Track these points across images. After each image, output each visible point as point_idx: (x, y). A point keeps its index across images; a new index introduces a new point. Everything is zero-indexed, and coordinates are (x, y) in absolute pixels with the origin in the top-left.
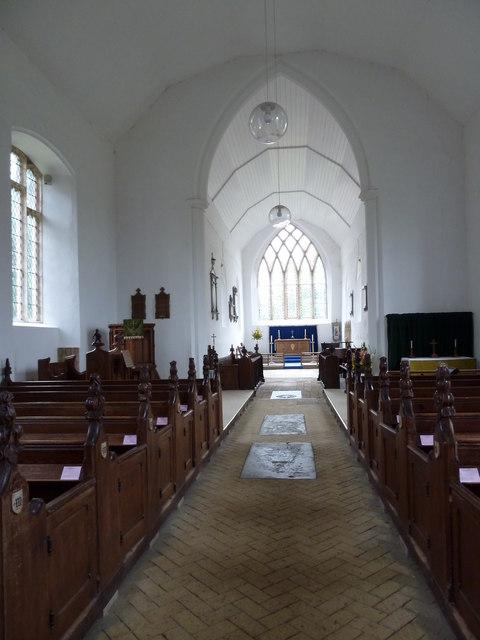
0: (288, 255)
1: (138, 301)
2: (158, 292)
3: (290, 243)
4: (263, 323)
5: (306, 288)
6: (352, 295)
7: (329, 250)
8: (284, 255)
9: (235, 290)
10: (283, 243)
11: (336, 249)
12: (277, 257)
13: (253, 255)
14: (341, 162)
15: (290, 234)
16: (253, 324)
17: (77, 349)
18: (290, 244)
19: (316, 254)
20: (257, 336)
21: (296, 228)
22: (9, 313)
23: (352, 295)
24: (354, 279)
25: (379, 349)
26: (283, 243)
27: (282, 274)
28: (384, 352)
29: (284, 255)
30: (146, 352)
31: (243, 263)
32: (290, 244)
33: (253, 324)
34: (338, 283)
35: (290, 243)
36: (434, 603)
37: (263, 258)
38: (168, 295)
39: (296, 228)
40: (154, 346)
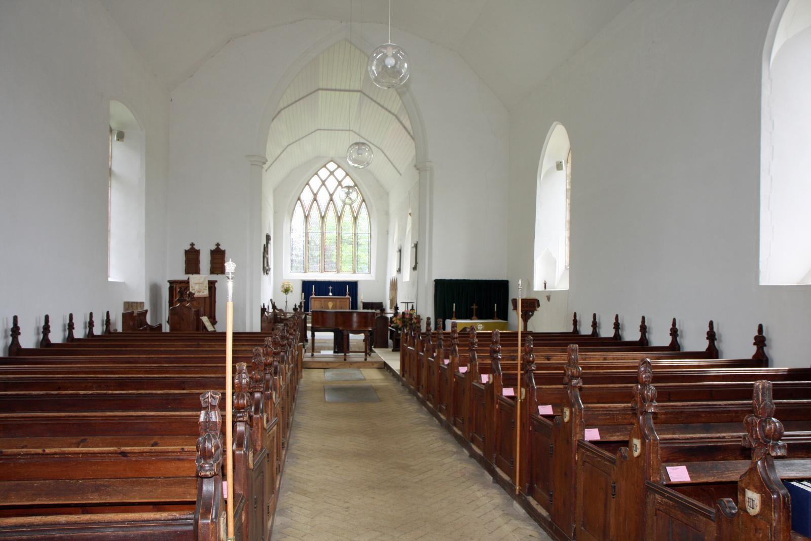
0: (328, 198)
1: (192, 259)
2: (214, 247)
3: (332, 183)
4: (296, 277)
5: (347, 234)
6: (400, 251)
7: (372, 193)
8: (323, 198)
9: (268, 238)
10: (323, 183)
11: (383, 194)
12: (315, 199)
13: (289, 197)
14: (396, 113)
15: (332, 173)
16: (285, 277)
17: (143, 303)
18: (329, 184)
19: (360, 199)
20: (286, 291)
21: (339, 166)
22: (107, 276)
23: (400, 251)
24: (401, 234)
25: (426, 310)
26: (323, 183)
27: (320, 219)
28: (548, 514)
29: (323, 198)
30: (354, 291)
31: (275, 206)
32: (329, 184)
33: (285, 277)
34: (385, 234)
35: (332, 183)
36: (422, 319)
37: (299, 199)
38: (755, 344)
39: (339, 166)
40: (215, 302)
